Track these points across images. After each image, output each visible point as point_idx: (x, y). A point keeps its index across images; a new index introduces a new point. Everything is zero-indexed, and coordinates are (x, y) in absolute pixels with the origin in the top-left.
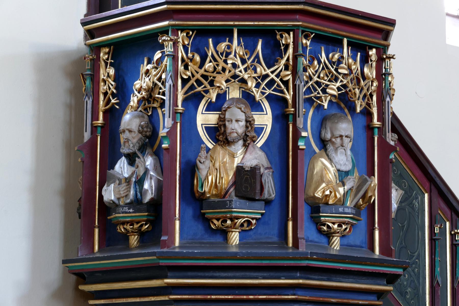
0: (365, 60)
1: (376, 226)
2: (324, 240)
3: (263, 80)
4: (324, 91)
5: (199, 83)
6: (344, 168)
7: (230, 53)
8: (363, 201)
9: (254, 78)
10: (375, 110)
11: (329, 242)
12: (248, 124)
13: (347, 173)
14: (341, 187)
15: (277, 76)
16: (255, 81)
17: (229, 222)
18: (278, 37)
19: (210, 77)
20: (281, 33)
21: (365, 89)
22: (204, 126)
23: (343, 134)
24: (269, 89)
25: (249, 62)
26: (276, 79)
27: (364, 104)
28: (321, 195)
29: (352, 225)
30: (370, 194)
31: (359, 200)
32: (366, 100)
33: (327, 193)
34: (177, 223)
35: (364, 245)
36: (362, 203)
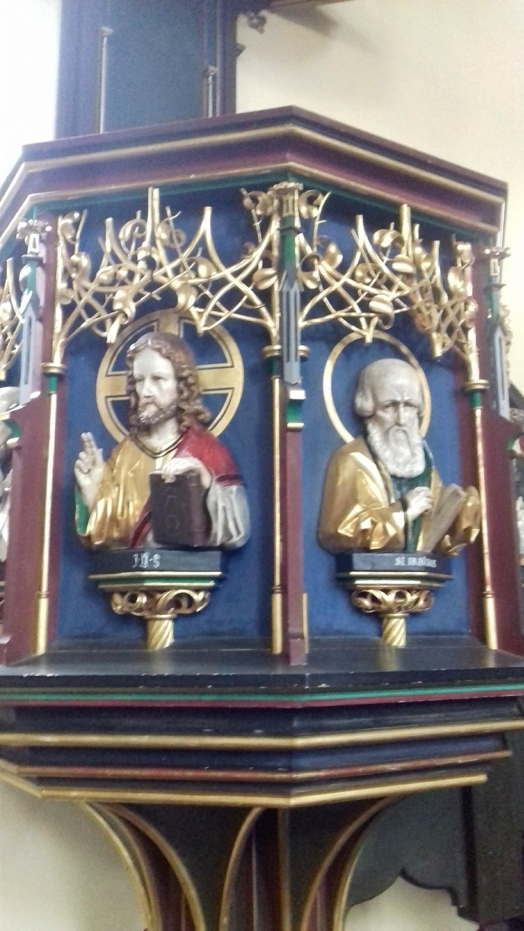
0: (449, 261)
1: (489, 589)
2: (368, 629)
3: (214, 291)
4: (364, 306)
5: (90, 310)
6: (404, 471)
7: (143, 239)
8: (452, 540)
9: (196, 286)
10: (473, 359)
11: (381, 631)
12: (181, 385)
13: (412, 482)
14: (398, 511)
15: (247, 281)
16: (195, 291)
17: (142, 600)
18: (247, 202)
19: (363, 292)
20: (253, 193)
21: (452, 314)
22: (110, 400)
23: (399, 399)
24: (230, 308)
25: (184, 256)
26: (243, 288)
27: (449, 343)
28: (352, 531)
29: (433, 591)
30: (465, 524)
31: (443, 538)
32: (455, 336)
33: (366, 525)
34: (44, 604)
35: (464, 629)
36: (449, 544)
